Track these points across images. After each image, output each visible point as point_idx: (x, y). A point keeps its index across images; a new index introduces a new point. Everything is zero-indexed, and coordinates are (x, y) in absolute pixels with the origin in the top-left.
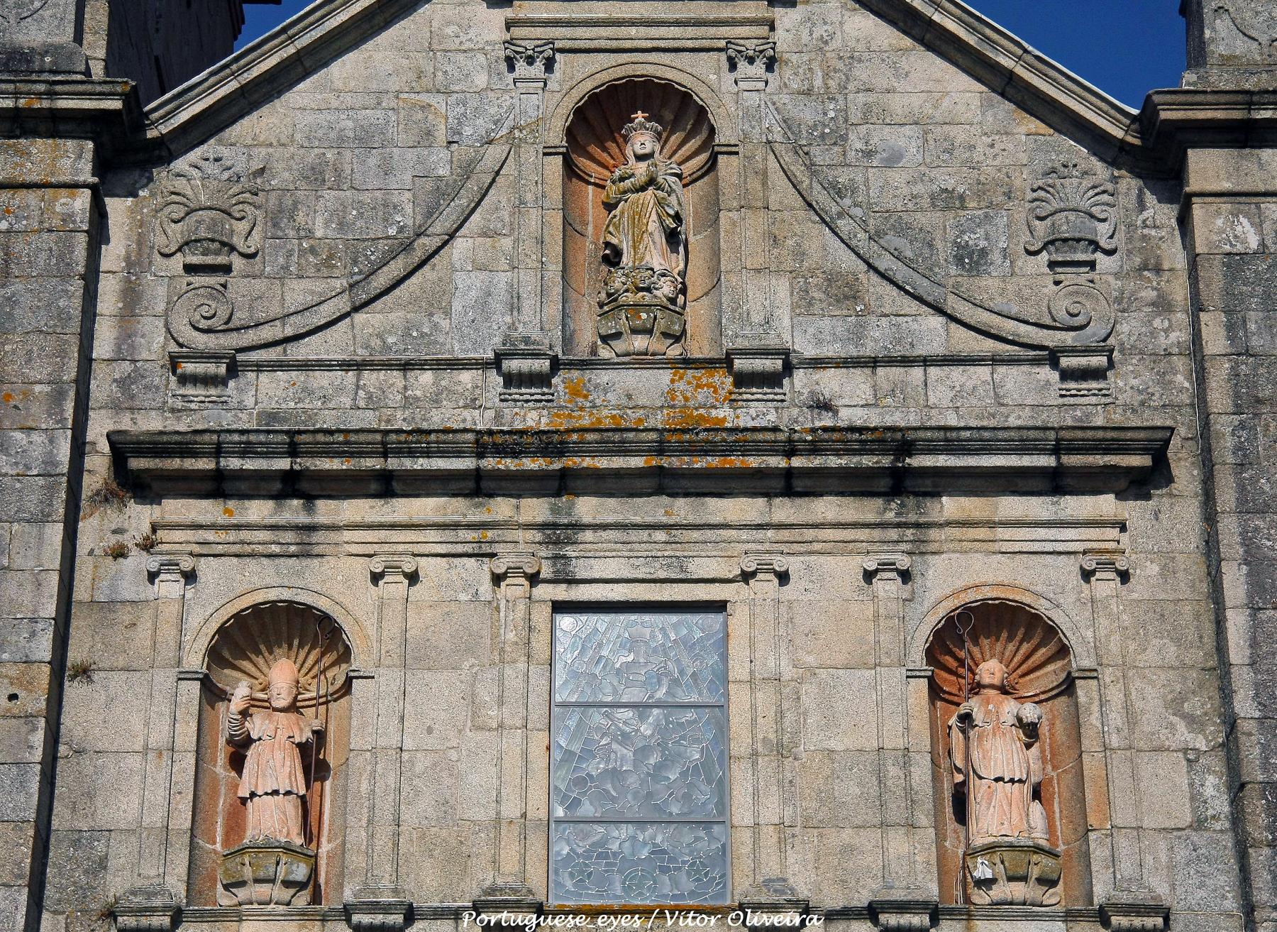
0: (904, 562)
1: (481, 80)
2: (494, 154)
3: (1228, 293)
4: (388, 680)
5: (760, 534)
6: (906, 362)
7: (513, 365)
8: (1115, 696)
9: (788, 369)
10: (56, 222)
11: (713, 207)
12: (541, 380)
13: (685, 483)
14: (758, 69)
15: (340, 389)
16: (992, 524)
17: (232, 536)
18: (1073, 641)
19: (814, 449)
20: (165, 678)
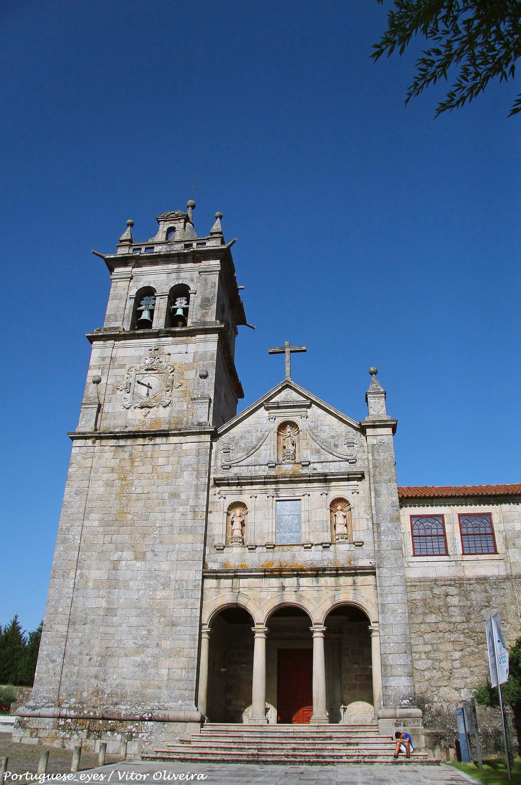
0: (326, 492)
1: (265, 422)
2: (267, 433)
3: (372, 450)
4: (253, 512)
5: (306, 489)
6: (327, 462)
7: (270, 465)
8: (357, 511)
9: (310, 464)
10: (205, 447)
11: (299, 440)
12: (274, 467)
13: (295, 482)
14: (305, 418)
15: (83, 766)
16: (339, 486)
17: (231, 492)
18: (350, 503)
19: (313, 476)
20: (222, 513)
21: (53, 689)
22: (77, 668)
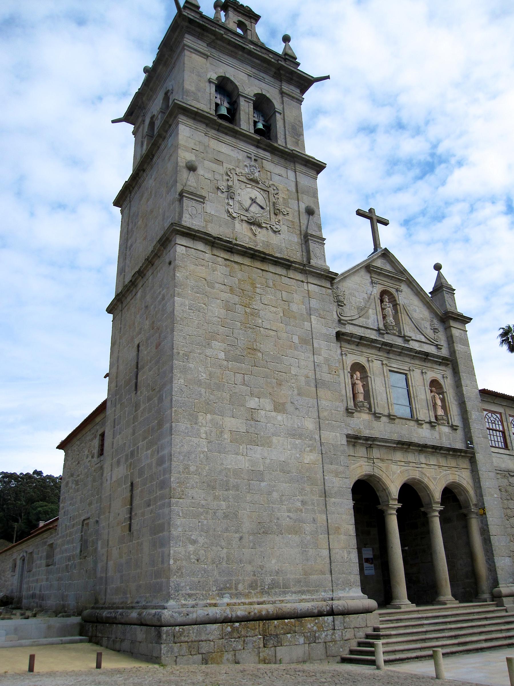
21: (199, 582)
22: (225, 550)
